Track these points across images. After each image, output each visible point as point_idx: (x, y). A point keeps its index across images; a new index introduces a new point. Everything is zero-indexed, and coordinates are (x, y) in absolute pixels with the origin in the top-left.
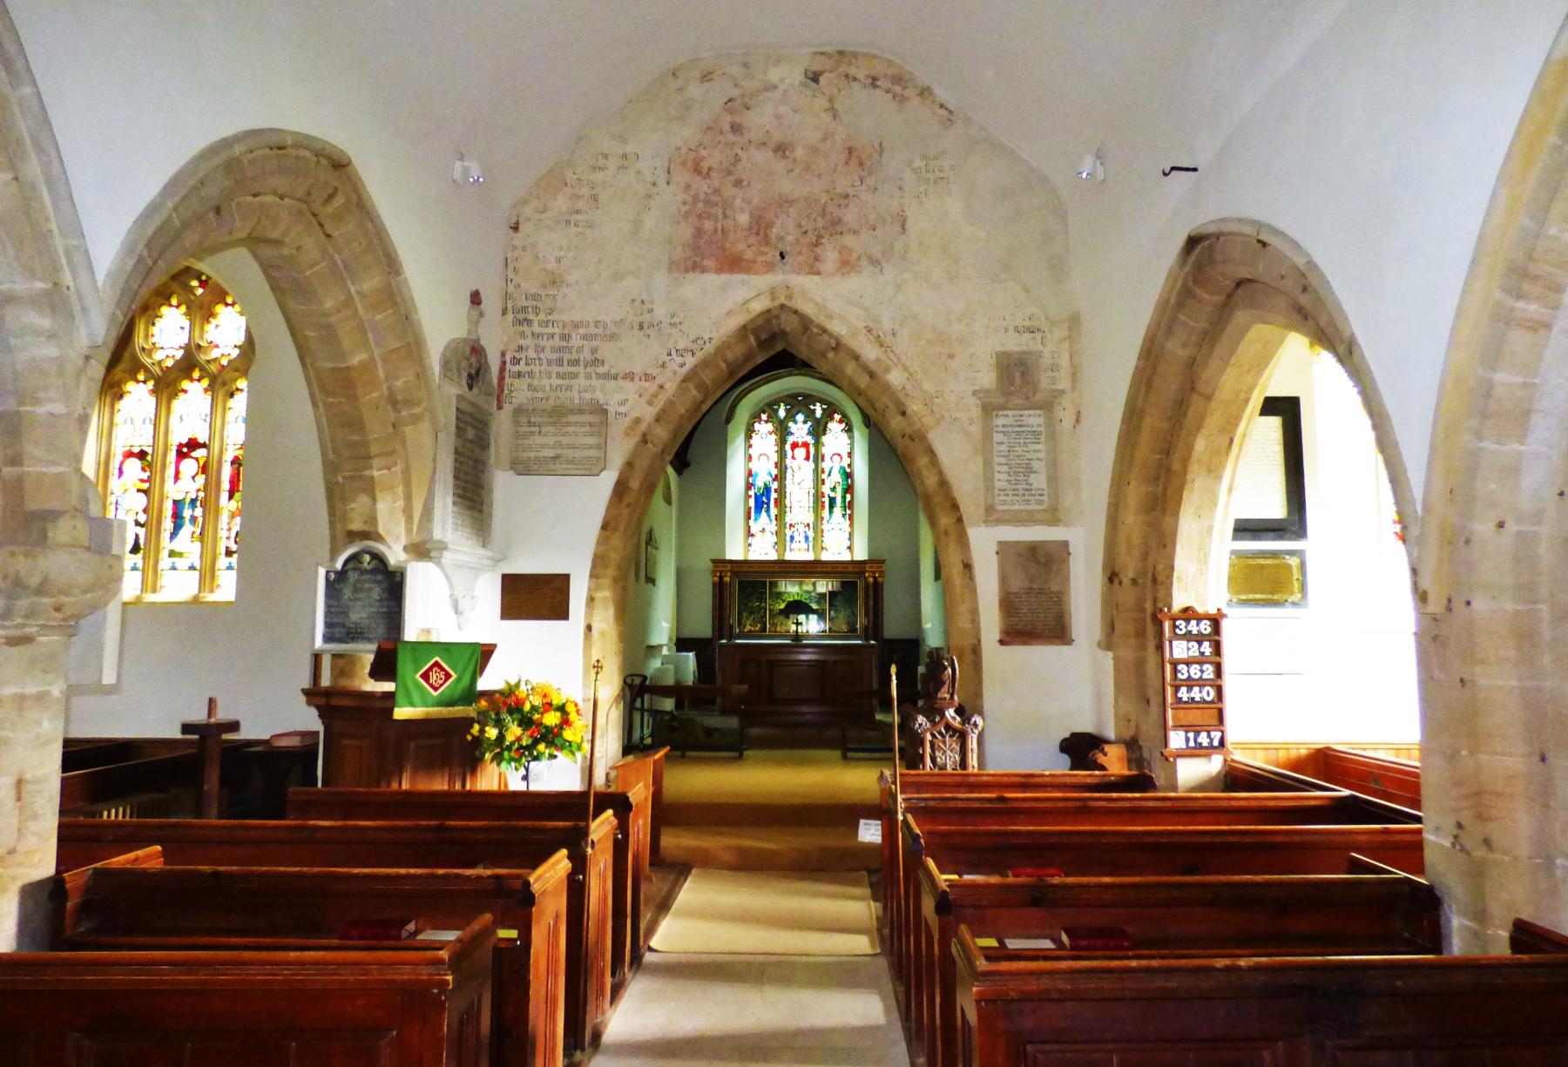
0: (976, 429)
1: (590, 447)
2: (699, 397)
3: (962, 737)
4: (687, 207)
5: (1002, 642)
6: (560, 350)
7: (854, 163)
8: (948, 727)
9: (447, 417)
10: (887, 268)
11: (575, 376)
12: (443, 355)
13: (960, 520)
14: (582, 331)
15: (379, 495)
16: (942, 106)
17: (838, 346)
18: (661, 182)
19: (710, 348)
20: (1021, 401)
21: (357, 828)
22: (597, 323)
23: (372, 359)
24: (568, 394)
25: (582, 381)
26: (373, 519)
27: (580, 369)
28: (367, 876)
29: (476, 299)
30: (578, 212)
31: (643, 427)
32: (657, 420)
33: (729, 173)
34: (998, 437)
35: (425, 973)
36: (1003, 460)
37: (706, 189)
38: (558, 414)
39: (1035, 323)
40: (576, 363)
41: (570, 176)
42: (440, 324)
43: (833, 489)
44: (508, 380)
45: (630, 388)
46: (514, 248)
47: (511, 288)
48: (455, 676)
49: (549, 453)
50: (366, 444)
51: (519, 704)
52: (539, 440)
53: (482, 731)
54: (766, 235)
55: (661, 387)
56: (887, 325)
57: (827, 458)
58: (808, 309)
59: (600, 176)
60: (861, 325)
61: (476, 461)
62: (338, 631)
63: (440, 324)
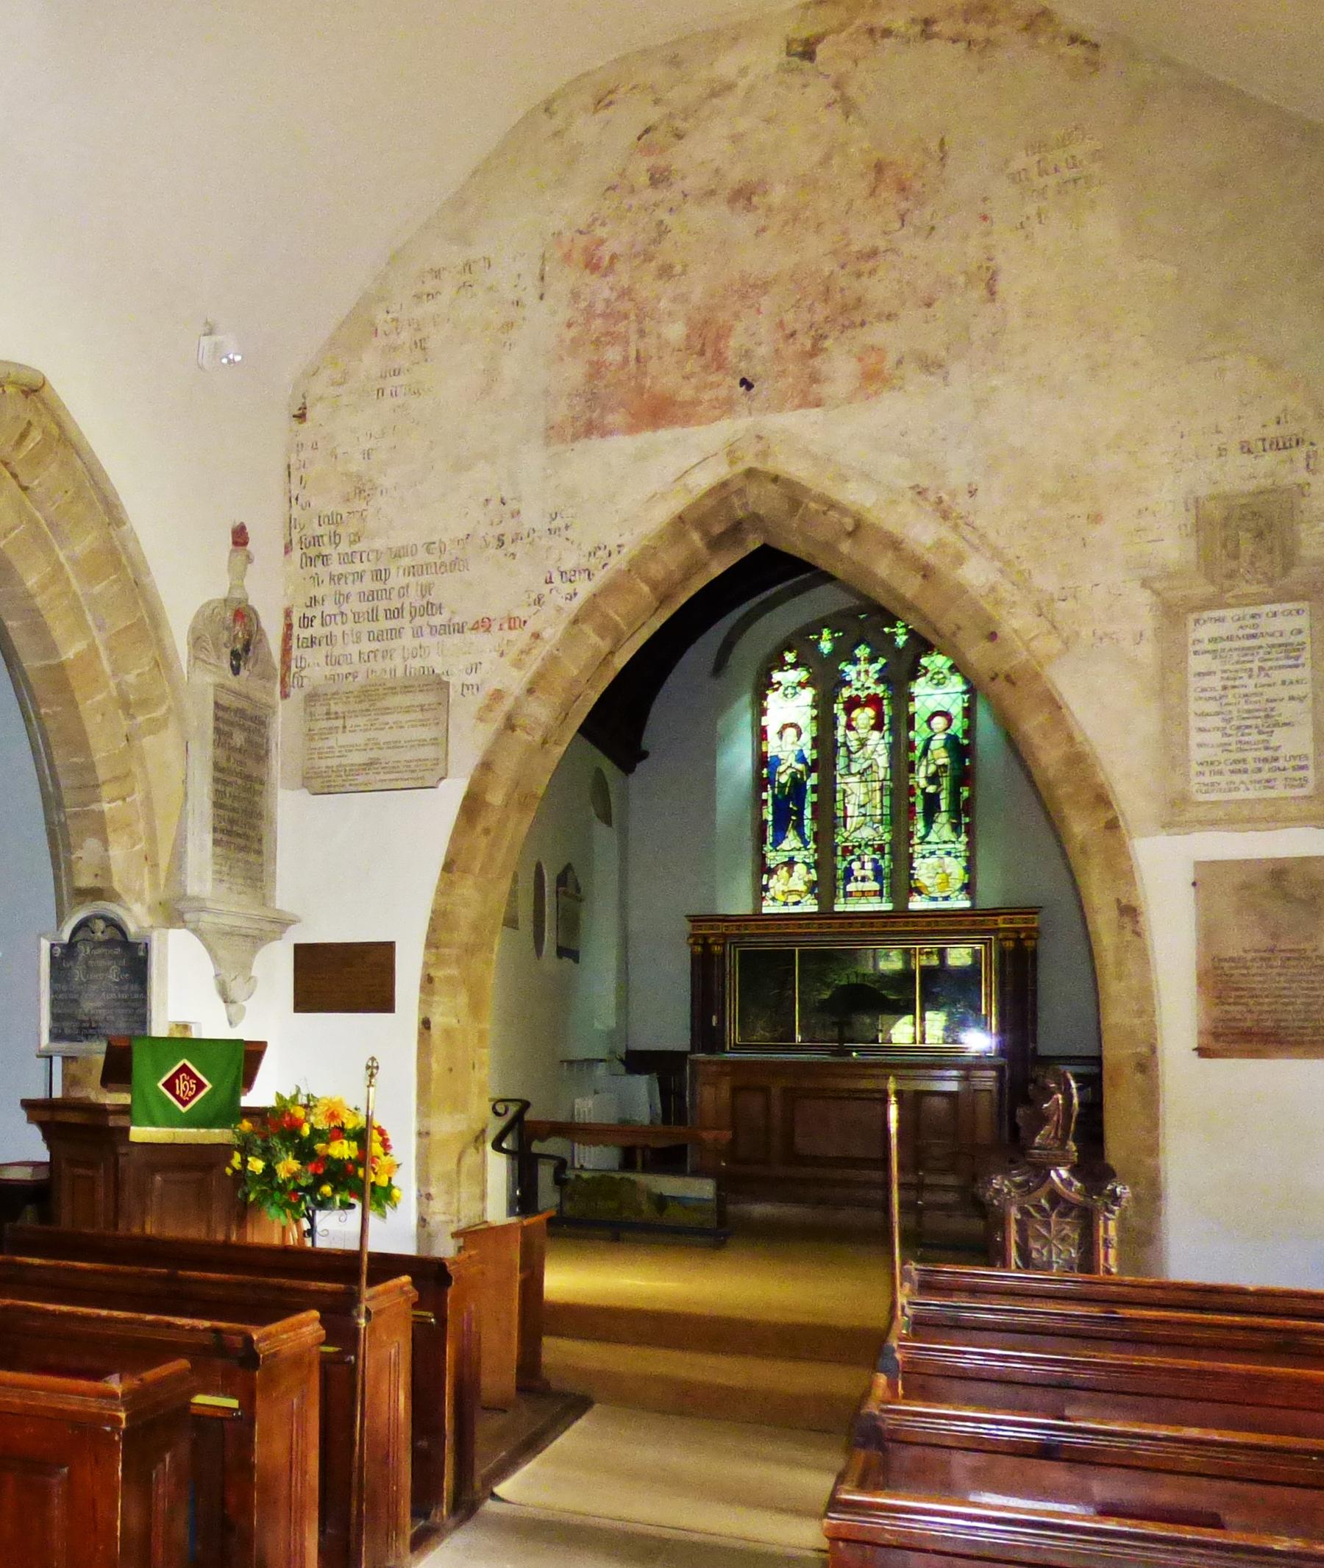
0: (1147, 652)
1: (422, 743)
2: (605, 645)
3: (1087, 1221)
4: (573, 332)
5: (1203, 1052)
6: (373, 596)
7: (887, 194)
8: (1055, 1198)
9: (202, 719)
10: (957, 370)
11: (398, 633)
12: (193, 629)
13: (1112, 825)
14: (407, 561)
15: (111, 837)
16: (1073, 40)
17: (858, 529)
18: (530, 297)
19: (619, 562)
20: (1254, 589)
21: (75, 1270)
22: (429, 546)
23: (92, 648)
24: (388, 664)
25: (407, 640)
26: (104, 870)
27: (404, 622)
28: (63, 1314)
29: (240, 537)
30: (396, 373)
31: (507, 704)
32: (530, 691)
33: (649, 258)
34: (1196, 663)
35: (94, 1405)
36: (1212, 707)
37: (606, 293)
38: (371, 696)
39: (1293, 429)
40: (398, 613)
41: (381, 318)
42: (186, 587)
43: (933, 779)
44: (295, 652)
45: (485, 643)
46: (300, 446)
47: (296, 512)
48: (209, 1086)
49: (357, 758)
50: (90, 768)
51: (295, 1126)
52: (343, 739)
53: (244, 1162)
54: (719, 354)
55: (536, 636)
56: (957, 478)
57: (919, 722)
58: (797, 470)
59: (429, 307)
60: (905, 484)
61: (248, 778)
62: (68, 1027)
63: (186, 587)
